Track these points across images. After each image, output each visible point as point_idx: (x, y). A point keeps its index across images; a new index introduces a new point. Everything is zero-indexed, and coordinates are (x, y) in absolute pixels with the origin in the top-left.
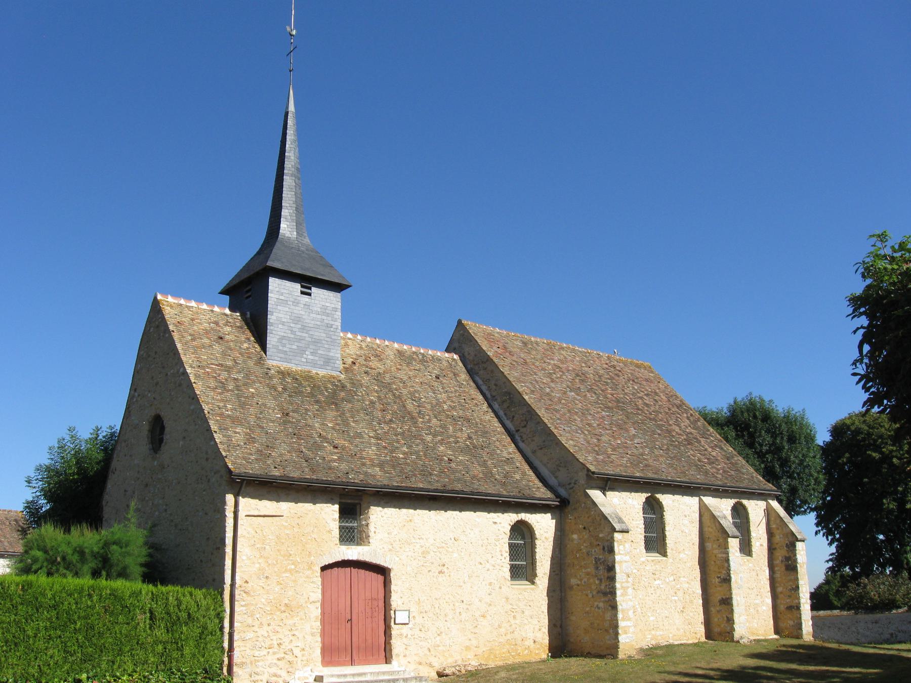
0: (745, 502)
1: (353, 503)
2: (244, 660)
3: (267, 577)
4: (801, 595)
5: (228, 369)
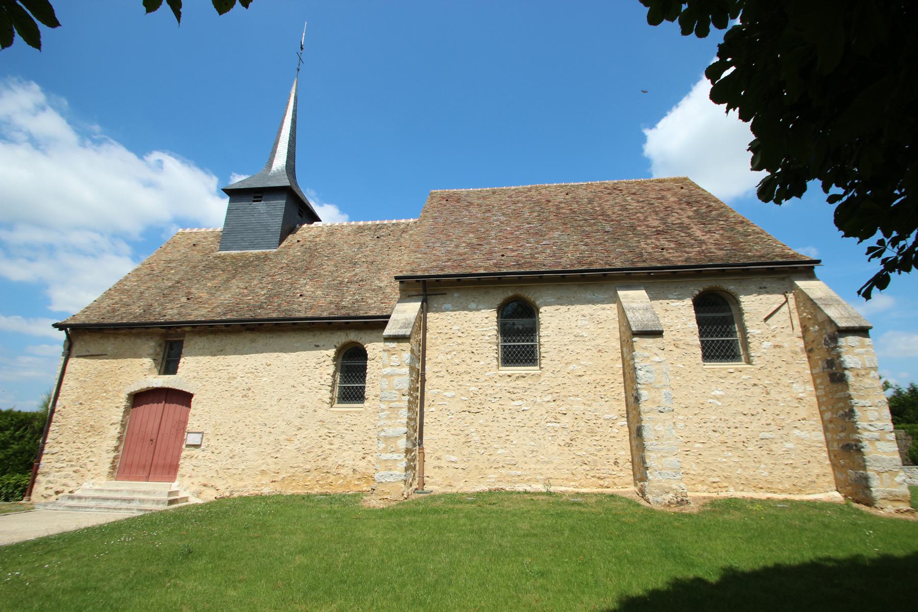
0: (730, 287)
2: (48, 470)
3: (81, 404)
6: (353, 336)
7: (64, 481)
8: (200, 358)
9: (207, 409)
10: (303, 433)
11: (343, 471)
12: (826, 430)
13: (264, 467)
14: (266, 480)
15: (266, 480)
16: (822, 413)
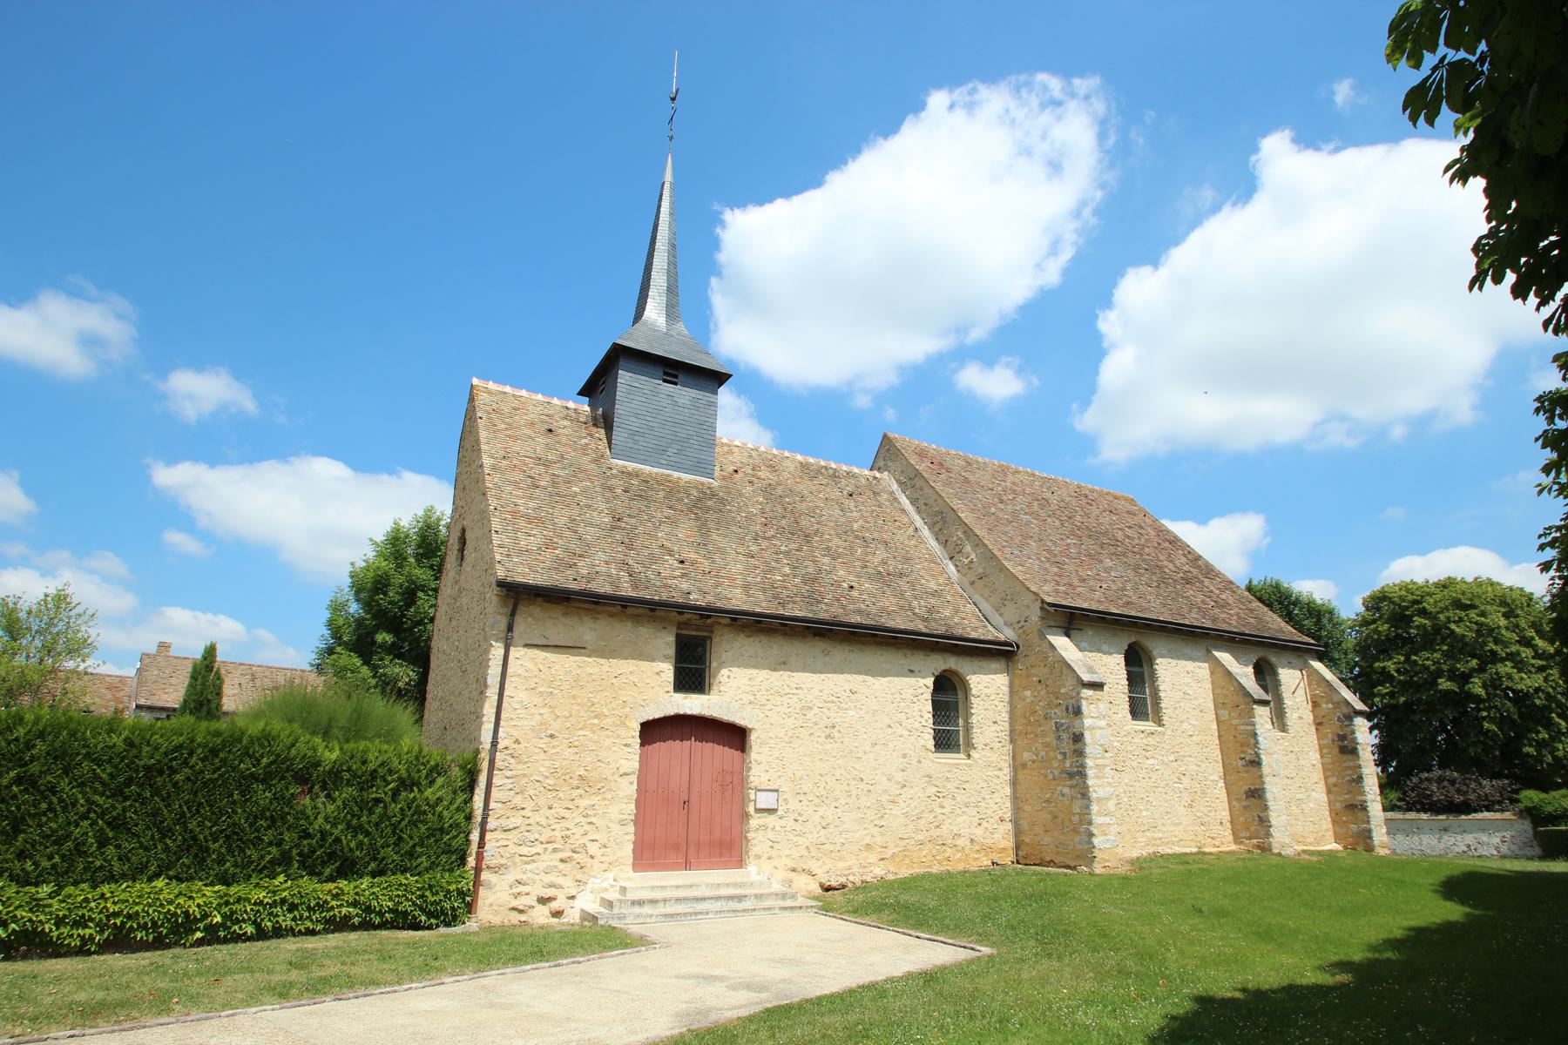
0: (1273, 659)
2: (503, 861)
3: (552, 736)
4: (1367, 789)
6: (952, 663)
7: (548, 879)
8: (754, 672)
9: (776, 754)
11: (960, 842)
12: (1329, 792)
13: (868, 840)
14: (873, 858)
15: (873, 858)
16: (1326, 778)
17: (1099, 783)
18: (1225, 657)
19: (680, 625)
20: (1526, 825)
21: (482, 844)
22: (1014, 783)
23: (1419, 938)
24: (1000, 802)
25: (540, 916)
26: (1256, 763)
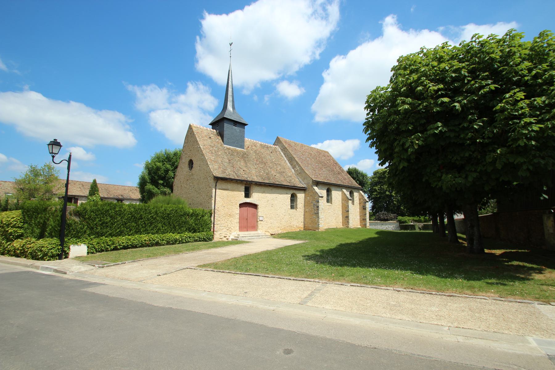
1: (248, 187)
5: (213, 147)
10: (285, 217)
14: (279, 229)
17: (321, 215)
18: (344, 190)
19: (245, 184)
20: (398, 223)
21: (214, 227)
22: (304, 215)
23: (370, 239)
24: (302, 219)
25: (225, 239)
26: (348, 211)
